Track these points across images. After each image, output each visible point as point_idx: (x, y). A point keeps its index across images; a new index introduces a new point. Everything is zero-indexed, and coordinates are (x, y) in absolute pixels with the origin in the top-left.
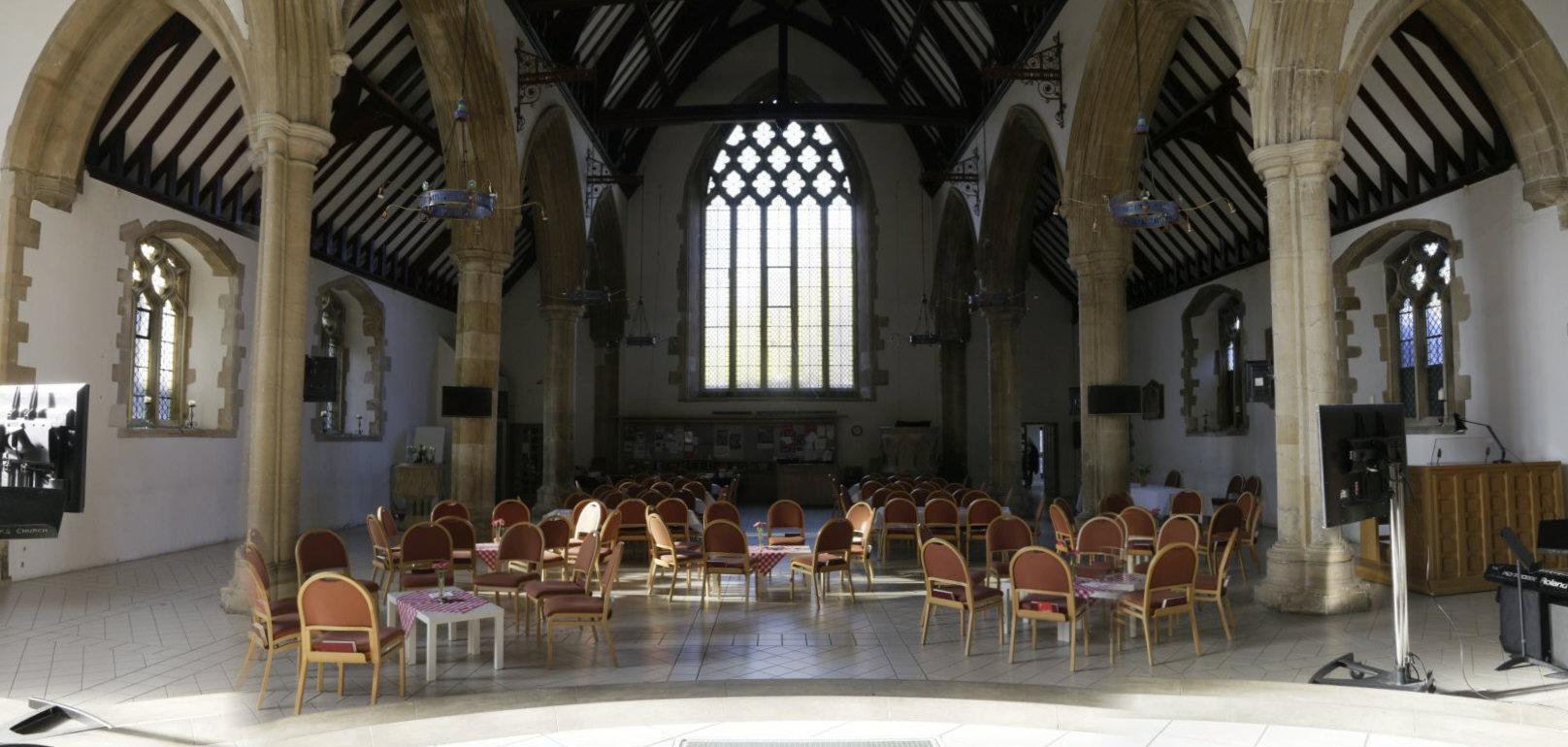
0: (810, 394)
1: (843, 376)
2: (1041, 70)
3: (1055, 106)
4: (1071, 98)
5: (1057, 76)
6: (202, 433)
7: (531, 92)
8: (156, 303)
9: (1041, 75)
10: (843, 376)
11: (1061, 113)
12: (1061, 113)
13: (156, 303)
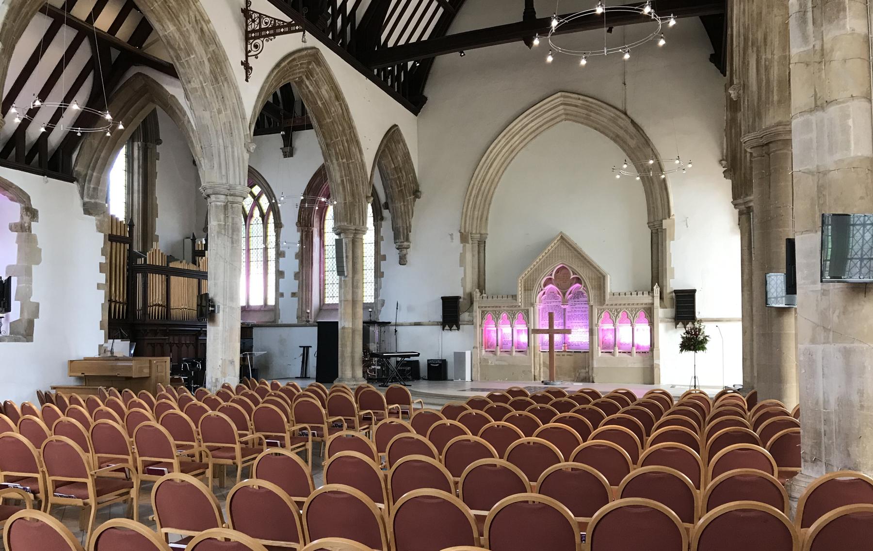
1: (271, 302)
7: (256, 46)
10: (271, 302)
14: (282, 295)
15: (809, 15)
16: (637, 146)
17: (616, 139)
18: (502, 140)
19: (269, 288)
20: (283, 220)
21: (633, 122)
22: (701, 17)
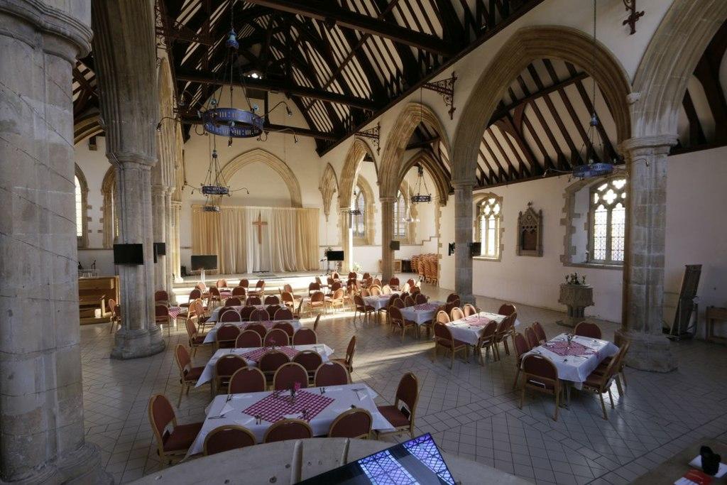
2: (373, 135)
3: (449, 108)
4: (383, 146)
5: (378, 137)
6: (416, 245)
9: (373, 136)
11: (379, 149)
12: (452, 110)
14: (266, 223)
15: (462, 195)
16: (290, 176)
17: (280, 173)
18: (231, 165)
19: (390, 66)
20: (89, 186)
21: (289, 168)
22: (316, 140)
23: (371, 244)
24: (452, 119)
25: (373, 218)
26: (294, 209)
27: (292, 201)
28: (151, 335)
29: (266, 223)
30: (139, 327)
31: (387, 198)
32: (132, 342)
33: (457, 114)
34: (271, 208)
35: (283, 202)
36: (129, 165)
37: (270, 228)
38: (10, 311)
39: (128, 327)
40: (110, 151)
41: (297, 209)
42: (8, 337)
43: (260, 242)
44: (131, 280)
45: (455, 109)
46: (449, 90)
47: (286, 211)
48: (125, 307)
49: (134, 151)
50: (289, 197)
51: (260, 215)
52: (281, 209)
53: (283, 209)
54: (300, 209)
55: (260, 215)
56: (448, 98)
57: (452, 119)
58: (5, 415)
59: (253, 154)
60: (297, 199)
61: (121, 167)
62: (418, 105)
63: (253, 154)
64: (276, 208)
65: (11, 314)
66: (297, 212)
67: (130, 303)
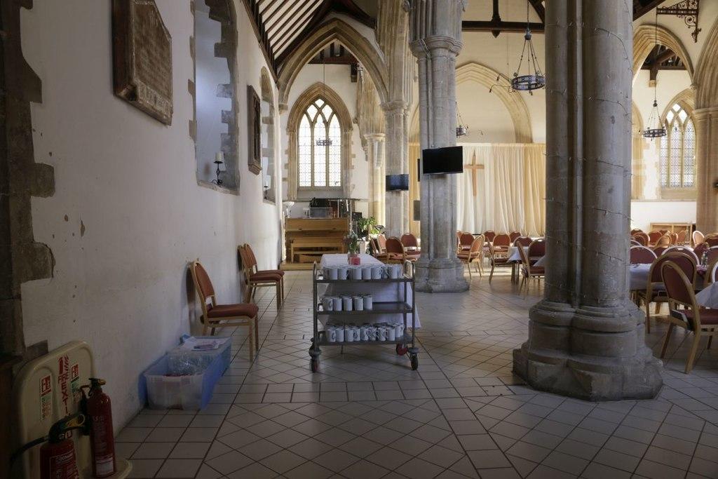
0: (320, 189)
3: (693, 29)
8: (327, 124)
12: (696, 33)
13: (327, 124)
14: (482, 166)
23: (637, 199)
24: (696, 41)
25: (641, 157)
26: (522, 145)
27: (516, 134)
28: (457, 267)
29: (482, 166)
30: (445, 255)
31: (710, 109)
32: (441, 272)
33: (702, 37)
34: (489, 145)
35: (503, 136)
36: (441, 52)
37: (488, 173)
38: (613, 117)
39: (432, 254)
40: (415, 38)
41: (527, 145)
42: (610, 146)
43: (475, 194)
44: (439, 194)
45: (700, 30)
46: (692, 10)
47: (510, 149)
48: (429, 230)
49: (447, 34)
50: (511, 126)
51: (474, 155)
52: (502, 145)
53: (507, 145)
54: (531, 145)
55: (474, 155)
56: (690, 20)
57: (696, 41)
58: (602, 233)
59: (464, 70)
60: (524, 131)
61: (429, 55)
62: (652, 27)
63: (464, 70)
64: (496, 145)
65: (613, 122)
66: (526, 149)
67: (435, 224)
